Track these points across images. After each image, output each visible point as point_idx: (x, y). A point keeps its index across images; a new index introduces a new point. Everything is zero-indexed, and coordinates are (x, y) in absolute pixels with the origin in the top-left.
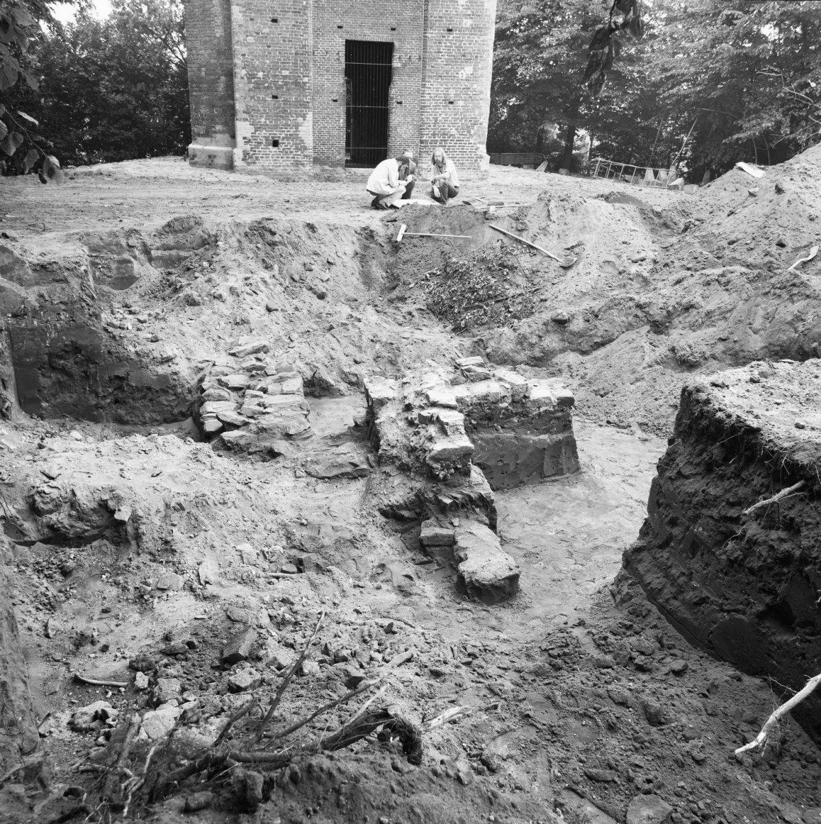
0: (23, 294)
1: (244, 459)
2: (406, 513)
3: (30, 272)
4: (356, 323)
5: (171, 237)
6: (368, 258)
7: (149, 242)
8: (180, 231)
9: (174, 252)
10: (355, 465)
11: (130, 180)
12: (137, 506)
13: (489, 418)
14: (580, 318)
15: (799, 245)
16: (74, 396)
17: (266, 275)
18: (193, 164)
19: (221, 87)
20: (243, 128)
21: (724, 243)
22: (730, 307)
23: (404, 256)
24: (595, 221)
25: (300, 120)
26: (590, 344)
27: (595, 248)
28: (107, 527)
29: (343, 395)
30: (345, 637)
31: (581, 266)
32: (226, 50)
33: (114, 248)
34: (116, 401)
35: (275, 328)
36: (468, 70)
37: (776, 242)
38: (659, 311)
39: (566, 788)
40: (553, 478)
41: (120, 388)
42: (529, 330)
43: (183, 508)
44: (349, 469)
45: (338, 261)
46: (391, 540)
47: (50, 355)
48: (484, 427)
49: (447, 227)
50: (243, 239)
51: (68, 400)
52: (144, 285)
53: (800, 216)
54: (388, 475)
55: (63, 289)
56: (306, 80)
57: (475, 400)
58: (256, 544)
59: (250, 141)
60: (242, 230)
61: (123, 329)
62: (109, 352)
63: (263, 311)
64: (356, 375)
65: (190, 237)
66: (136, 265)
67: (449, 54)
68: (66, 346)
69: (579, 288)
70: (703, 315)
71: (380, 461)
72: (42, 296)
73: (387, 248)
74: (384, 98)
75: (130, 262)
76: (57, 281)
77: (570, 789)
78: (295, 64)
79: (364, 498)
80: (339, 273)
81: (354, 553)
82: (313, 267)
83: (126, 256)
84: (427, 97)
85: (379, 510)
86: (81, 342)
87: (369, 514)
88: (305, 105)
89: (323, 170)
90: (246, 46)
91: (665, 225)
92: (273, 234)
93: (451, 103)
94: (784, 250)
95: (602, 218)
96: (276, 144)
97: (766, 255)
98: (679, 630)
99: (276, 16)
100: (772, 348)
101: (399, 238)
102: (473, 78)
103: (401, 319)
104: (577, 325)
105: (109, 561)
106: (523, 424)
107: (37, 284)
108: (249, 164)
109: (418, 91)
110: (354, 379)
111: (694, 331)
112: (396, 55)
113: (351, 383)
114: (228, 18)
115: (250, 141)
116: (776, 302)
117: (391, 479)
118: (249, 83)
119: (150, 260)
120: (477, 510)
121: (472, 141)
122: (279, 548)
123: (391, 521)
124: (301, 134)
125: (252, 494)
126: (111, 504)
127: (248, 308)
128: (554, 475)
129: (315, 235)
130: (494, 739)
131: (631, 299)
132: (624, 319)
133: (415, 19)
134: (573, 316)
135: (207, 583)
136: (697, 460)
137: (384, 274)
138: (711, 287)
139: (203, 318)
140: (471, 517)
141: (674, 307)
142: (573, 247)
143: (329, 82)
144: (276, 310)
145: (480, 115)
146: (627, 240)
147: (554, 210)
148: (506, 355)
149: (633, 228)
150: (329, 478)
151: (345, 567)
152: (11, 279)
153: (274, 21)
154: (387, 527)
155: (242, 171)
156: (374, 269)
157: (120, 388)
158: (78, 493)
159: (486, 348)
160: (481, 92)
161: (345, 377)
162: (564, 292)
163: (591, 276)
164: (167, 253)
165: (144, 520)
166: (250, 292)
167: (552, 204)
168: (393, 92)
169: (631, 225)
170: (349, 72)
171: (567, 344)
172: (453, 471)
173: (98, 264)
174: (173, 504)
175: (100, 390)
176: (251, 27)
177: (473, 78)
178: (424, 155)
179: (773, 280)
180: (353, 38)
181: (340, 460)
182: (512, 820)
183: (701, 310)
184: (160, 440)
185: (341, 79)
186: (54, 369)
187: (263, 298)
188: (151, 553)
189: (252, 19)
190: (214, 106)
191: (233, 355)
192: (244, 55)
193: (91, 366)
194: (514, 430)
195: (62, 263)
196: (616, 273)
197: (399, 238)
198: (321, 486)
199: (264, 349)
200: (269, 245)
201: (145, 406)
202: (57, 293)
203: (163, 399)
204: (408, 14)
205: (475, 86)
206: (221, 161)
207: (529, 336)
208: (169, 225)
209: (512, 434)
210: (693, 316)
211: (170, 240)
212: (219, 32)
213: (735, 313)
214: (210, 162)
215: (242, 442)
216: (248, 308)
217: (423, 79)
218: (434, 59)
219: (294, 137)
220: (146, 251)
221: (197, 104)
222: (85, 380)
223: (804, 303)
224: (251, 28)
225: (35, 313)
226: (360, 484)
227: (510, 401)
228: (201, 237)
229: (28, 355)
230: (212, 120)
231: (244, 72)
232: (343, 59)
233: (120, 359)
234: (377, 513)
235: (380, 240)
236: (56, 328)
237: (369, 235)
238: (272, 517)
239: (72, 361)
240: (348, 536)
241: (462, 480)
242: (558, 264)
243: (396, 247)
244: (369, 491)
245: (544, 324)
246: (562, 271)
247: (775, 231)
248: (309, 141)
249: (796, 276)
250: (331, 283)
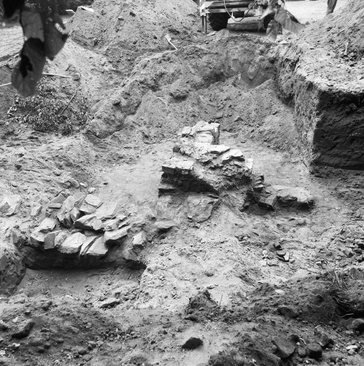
14: (122, 98)
26: (134, 108)
64: (68, 181)
69: (95, 86)
70: (171, 76)
71: (217, 193)
100: (205, 78)
104: (124, 103)
110: (69, 184)
111: (171, 84)
113: (69, 187)
136: (341, 113)
142: (68, 68)
171: (125, 113)
183: (168, 74)
207: (109, 117)
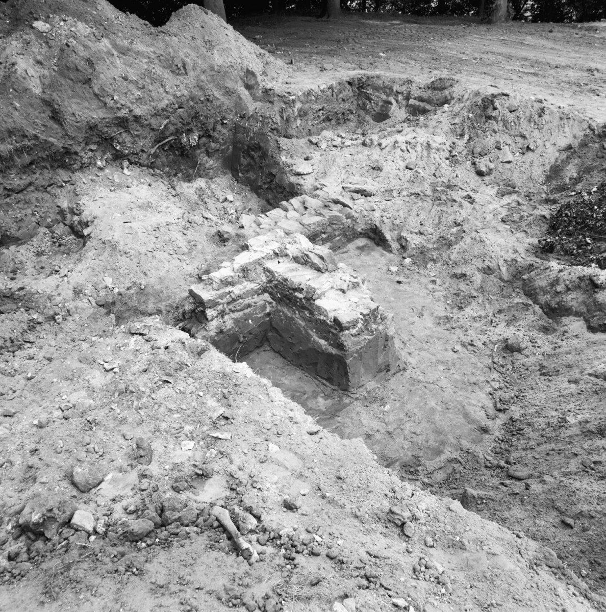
9: (422, 104)
29: (391, 252)
33: (388, 90)
40: (324, 381)
47: (248, 146)
64: (407, 241)
75: (391, 103)
83: (392, 99)
92: (495, 109)
110: (404, 244)
161: (400, 239)
173: (372, 100)
182: (445, 607)
209: (303, 324)
211: (426, 95)
228: (446, 97)
229: (240, 142)
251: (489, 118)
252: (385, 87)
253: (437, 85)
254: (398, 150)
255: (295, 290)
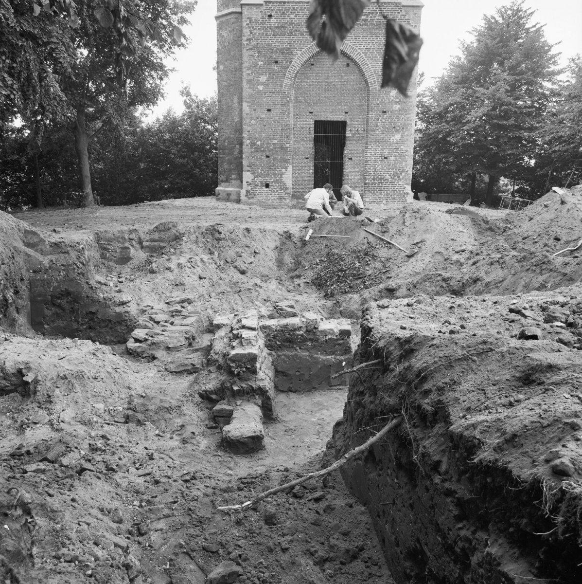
0: (41, 259)
1: (138, 361)
2: (214, 397)
3: (48, 247)
4: (258, 289)
5: (157, 234)
6: (283, 250)
7: (142, 236)
8: (163, 231)
9: (157, 244)
10: (194, 365)
11: (177, 208)
12: (39, 374)
13: (290, 341)
14: (405, 288)
15: (570, 239)
16: (65, 323)
17: (206, 257)
18: (218, 199)
19: (236, 152)
20: (247, 176)
21: (520, 239)
22: (501, 279)
23: (307, 249)
24: (435, 226)
25: (284, 170)
27: (432, 243)
28: (20, 386)
30: (126, 459)
31: (420, 255)
32: (239, 130)
33: (120, 240)
34: (90, 328)
35: (201, 289)
36: (398, 137)
37: (553, 237)
38: (457, 283)
39: (184, 553)
40: (338, 387)
41: (92, 319)
42: (369, 296)
43: (66, 378)
44: (190, 368)
45: (262, 252)
46: (201, 413)
47: (52, 296)
48: (286, 347)
49: (338, 231)
50: (199, 236)
51: (62, 325)
52: (135, 262)
53: (575, 219)
54: (210, 372)
55: (65, 257)
56: (288, 145)
57: (278, 328)
58: (108, 405)
59: (250, 184)
60: (201, 231)
61: (107, 285)
62: (87, 297)
63: (196, 278)
65: (168, 234)
66: (132, 250)
67: (384, 127)
68: (62, 291)
70: (484, 285)
72: (52, 261)
73: (299, 244)
74: (341, 156)
75: (129, 248)
76: (63, 253)
77: (187, 553)
78: (281, 136)
79: (191, 385)
80: (261, 259)
81: (168, 416)
82: (243, 254)
83: (127, 245)
84: (369, 155)
85: (199, 393)
86: (71, 289)
87: (191, 395)
88: (287, 161)
89: (298, 203)
90: (250, 126)
91: (490, 229)
92: (220, 233)
93: (386, 158)
94: (559, 242)
95: (440, 224)
96: (267, 186)
97: (545, 246)
98: (343, 478)
99: (270, 107)
101: (307, 238)
102: (401, 142)
103: (291, 288)
105: (15, 405)
106: (315, 347)
107: (51, 254)
108: (249, 198)
109: (363, 151)
112: (348, 129)
114: (241, 110)
115: (250, 184)
116: (532, 275)
117: (211, 374)
118: (252, 148)
119: (142, 248)
120: (257, 397)
121: (400, 183)
122: (121, 409)
123: (205, 401)
124: (284, 180)
125: (116, 376)
126: (24, 371)
127: (186, 276)
128: (339, 385)
129: (249, 235)
130: (159, 519)
131: (440, 275)
132: (434, 288)
133: (360, 106)
134: (399, 286)
135: (62, 422)
137: (293, 261)
138: (493, 266)
139: (156, 281)
140: (252, 400)
141: (467, 280)
142: (418, 243)
143: (303, 145)
144: (205, 278)
145: (406, 165)
146: (455, 238)
147: (408, 219)
148: (353, 312)
149: (461, 230)
150: (176, 372)
151: (157, 424)
152: (37, 251)
153: (269, 110)
154: (201, 405)
155: (246, 203)
156: (286, 257)
157: (92, 319)
158: (7, 364)
159: (340, 307)
160: (407, 151)
162: (403, 273)
163: (424, 262)
164: (152, 244)
165: (41, 383)
166: (190, 266)
167: (407, 215)
168: (346, 151)
169: (461, 228)
170: (317, 140)
172: (244, 369)
174: (61, 375)
175: (80, 320)
176: (254, 115)
177: (401, 142)
178: (367, 192)
179: (533, 261)
180: (319, 119)
181: (186, 362)
184: (79, 342)
185: (311, 145)
186: (54, 305)
187: (199, 271)
188: (39, 403)
189: (255, 110)
190: (231, 163)
191: (167, 303)
192: (249, 131)
193: (76, 304)
194: (308, 351)
195: (67, 242)
196: (442, 260)
197: (307, 238)
198: (170, 377)
199: (190, 302)
200: (217, 240)
201: (107, 332)
202: (61, 259)
203: (118, 328)
204: (356, 103)
205: (402, 147)
206: (233, 197)
208: (156, 227)
209: (307, 354)
210: (479, 286)
211: (156, 236)
212: (236, 119)
213: (505, 283)
214: (228, 198)
215: (139, 350)
216: (186, 276)
217: (367, 144)
218: (374, 131)
219: (280, 181)
220: (140, 242)
221: (222, 162)
222: (67, 309)
223: (548, 275)
224: (254, 115)
225: (46, 271)
226: (192, 378)
227: (305, 330)
229: (39, 295)
230: (230, 172)
231: (249, 141)
232: (313, 132)
233: (93, 301)
234: (197, 396)
235: (295, 240)
236: (57, 280)
237: (288, 236)
238: (127, 391)
239: (65, 301)
240: (167, 405)
241: (251, 376)
242: (404, 254)
243: (304, 243)
244: (195, 382)
245: (379, 292)
246: (406, 259)
247: (556, 230)
248: (289, 183)
249: (546, 256)
250: (253, 265)
251: (219, 240)
252: (117, 238)
253: (161, 228)
254: (186, 268)
255: (295, 330)
